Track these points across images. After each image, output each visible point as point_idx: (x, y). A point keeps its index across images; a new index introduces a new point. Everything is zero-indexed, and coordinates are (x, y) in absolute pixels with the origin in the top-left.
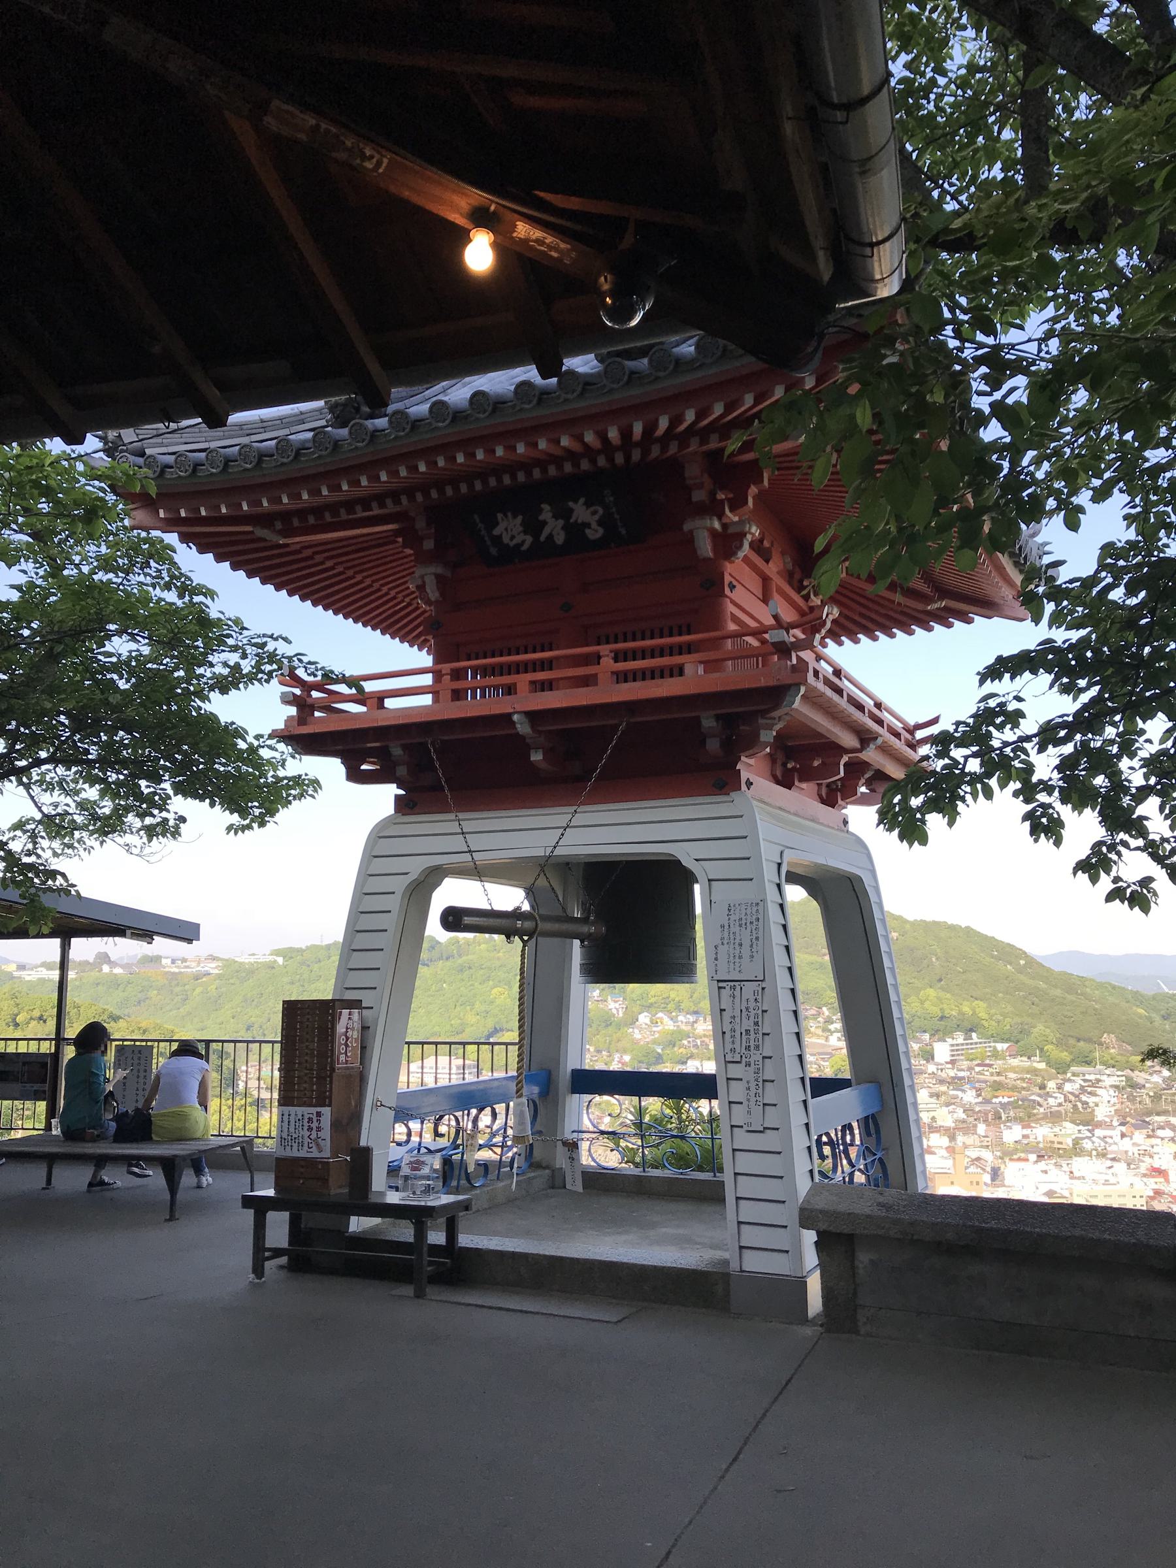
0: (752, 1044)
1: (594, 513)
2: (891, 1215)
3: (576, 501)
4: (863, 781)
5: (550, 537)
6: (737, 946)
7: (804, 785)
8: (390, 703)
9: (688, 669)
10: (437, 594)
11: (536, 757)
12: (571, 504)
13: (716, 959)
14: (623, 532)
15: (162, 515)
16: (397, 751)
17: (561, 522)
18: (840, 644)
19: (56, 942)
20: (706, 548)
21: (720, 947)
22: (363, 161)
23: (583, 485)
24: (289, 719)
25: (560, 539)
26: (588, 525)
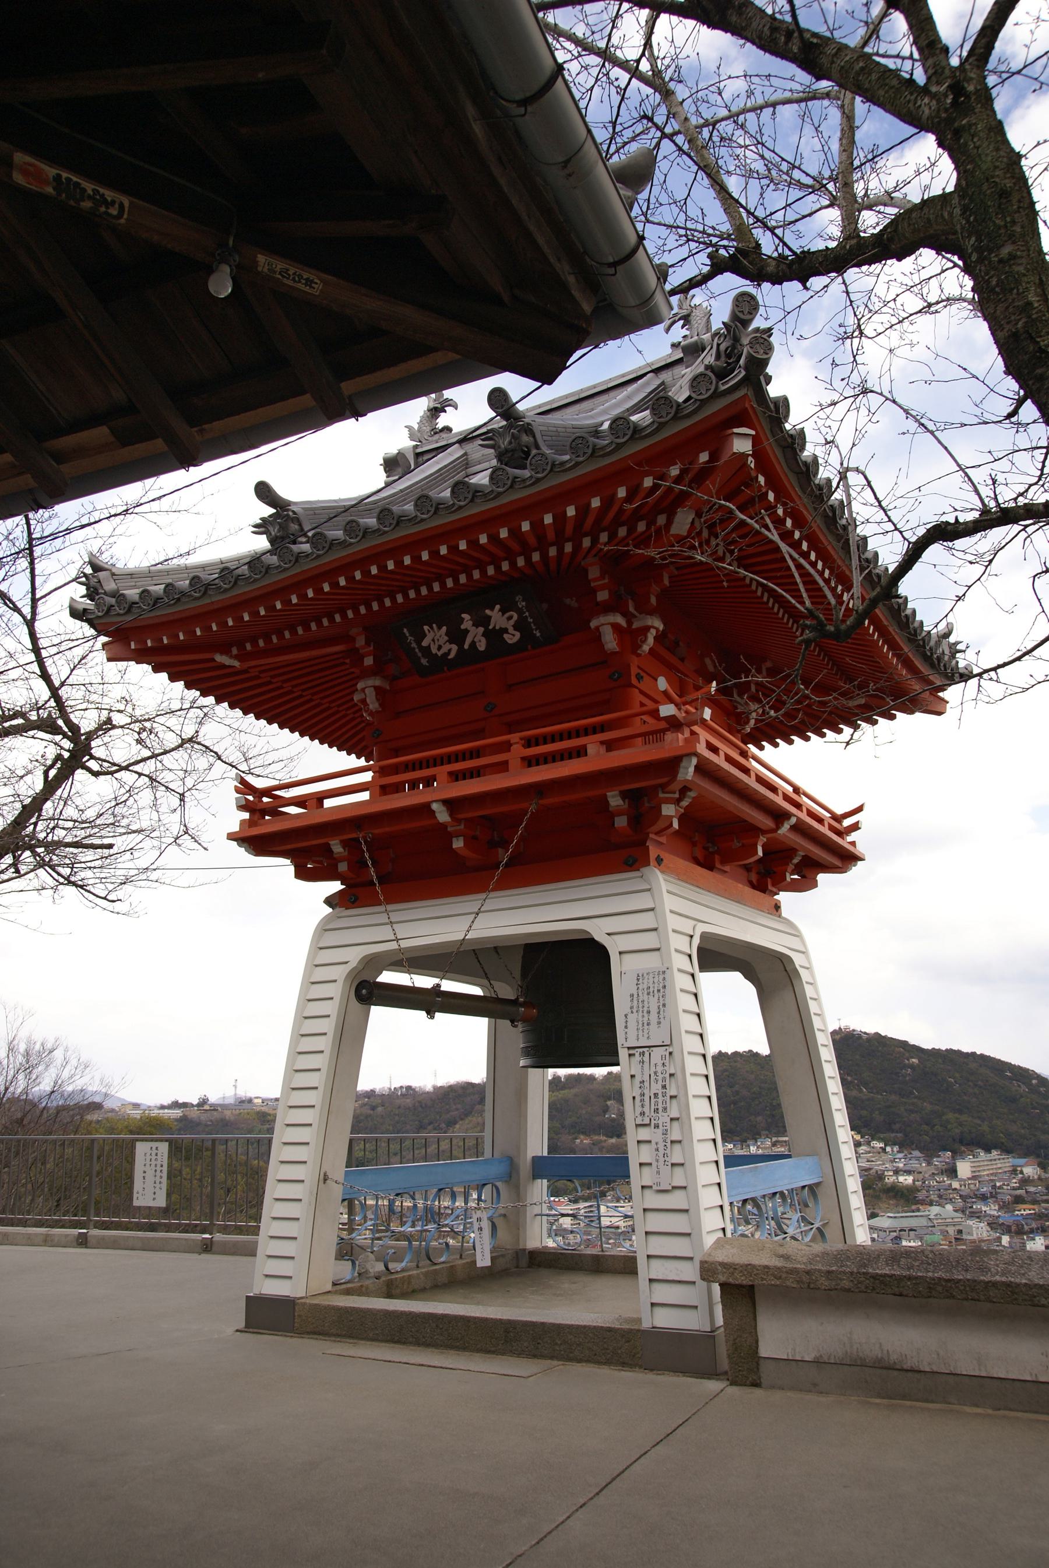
0: (660, 1107)
1: (510, 618)
2: (789, 1265)
3: (492, 609)
4: (791, 867)
5: (473, 644)
6: (645, 1014)
7: (727, 868)
8: (328, 803)
9: (591, 750)
10: (377, 705)
11: (458, 844)
12: (488, 612)
13: (626, 1027)
15: (133, 647)
16: (337, 848)
17: (481, 629)
18: (776, 745)
20: (610, 641)
21: (630, 1016)
22: (107, 208)
23: (498, 592)
24: (243, 822)
25: (482, 646)
26: (506, 631)
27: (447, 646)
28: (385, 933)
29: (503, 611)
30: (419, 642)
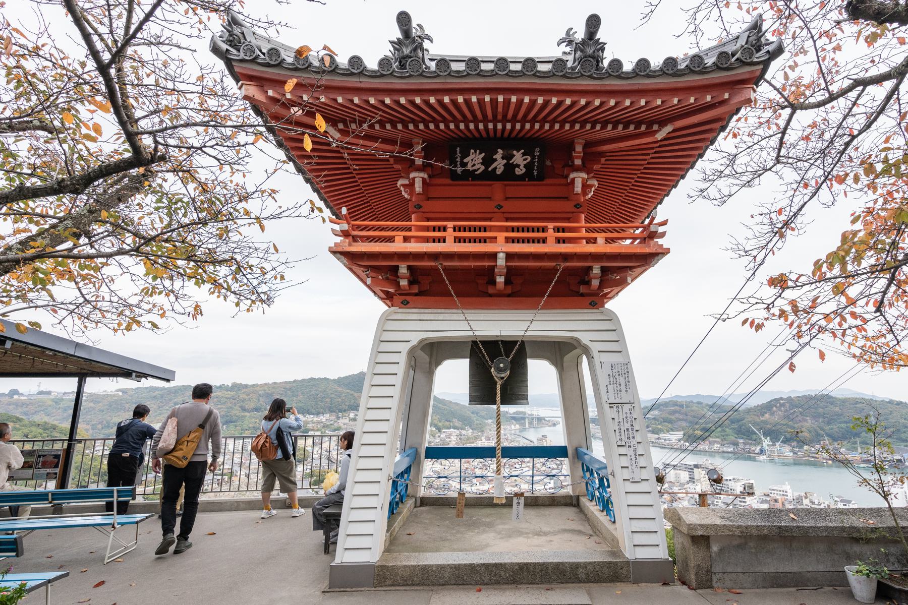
1: (525, 160)
12: (515, 152)
14: (535, 173)
17: (505, 161)
19: (75, 381)
23: (526, 143)
25: (499, 172)
27: (479, 166)
28: (464, 325)
29: (524, 154)
30: (462, 158)
